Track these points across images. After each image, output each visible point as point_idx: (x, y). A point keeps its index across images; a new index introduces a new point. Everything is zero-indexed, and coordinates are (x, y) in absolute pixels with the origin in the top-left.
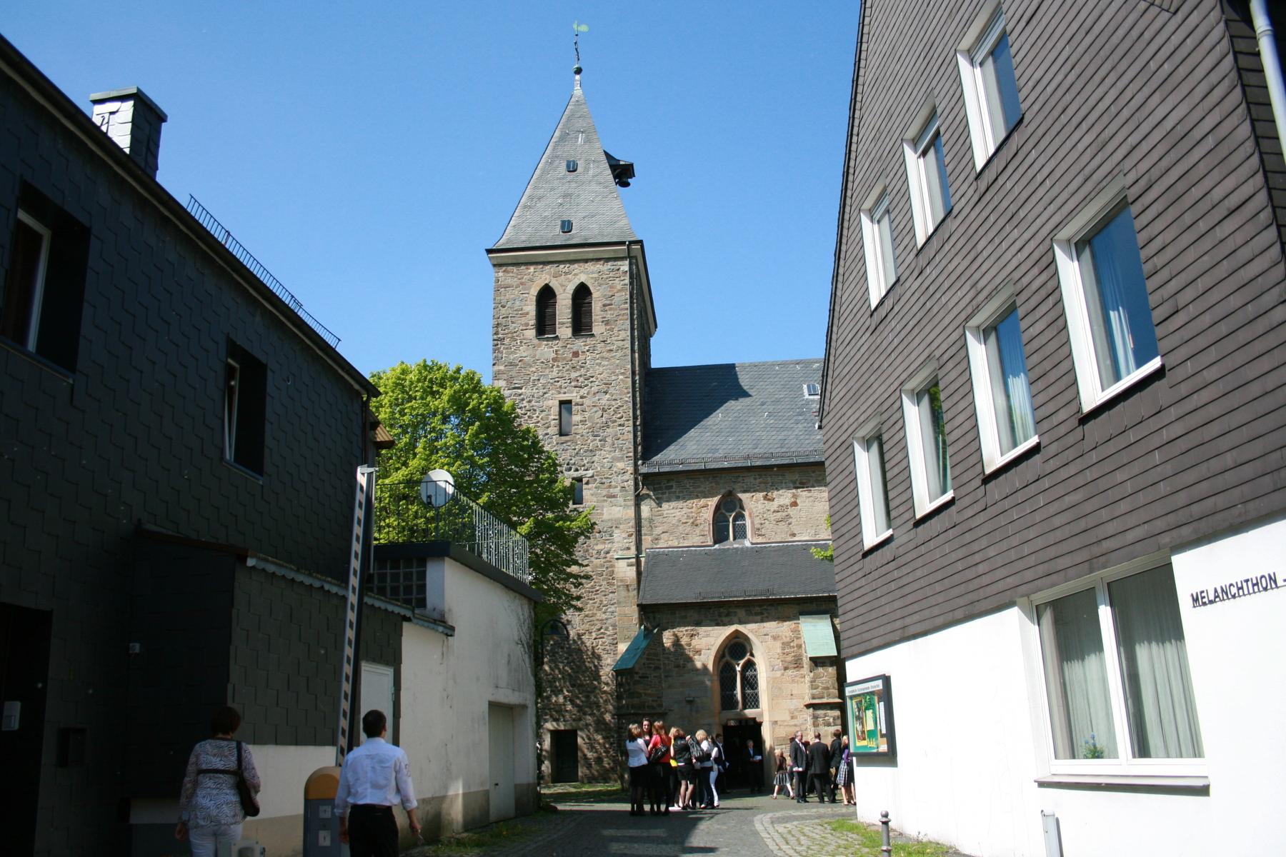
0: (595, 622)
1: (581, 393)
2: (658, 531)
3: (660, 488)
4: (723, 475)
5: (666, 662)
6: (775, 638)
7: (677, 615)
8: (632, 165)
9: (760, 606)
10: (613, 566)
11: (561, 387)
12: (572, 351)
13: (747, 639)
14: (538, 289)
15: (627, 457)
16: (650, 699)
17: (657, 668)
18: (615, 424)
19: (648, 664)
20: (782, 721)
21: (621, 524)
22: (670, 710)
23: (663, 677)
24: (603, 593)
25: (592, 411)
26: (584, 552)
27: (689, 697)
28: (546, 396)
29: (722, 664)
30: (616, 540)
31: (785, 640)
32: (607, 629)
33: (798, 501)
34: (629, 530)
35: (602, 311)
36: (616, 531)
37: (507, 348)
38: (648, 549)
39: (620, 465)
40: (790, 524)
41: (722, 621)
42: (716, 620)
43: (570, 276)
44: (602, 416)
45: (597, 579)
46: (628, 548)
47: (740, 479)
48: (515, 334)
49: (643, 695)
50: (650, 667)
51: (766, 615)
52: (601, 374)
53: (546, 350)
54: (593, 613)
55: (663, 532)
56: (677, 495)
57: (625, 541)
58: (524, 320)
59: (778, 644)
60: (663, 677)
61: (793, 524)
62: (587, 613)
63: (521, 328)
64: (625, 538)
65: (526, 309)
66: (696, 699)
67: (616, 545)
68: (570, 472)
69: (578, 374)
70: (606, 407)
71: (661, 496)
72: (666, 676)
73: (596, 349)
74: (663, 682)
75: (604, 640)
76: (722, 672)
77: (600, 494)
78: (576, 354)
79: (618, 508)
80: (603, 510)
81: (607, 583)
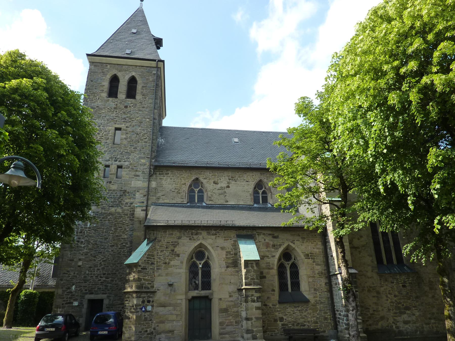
0: (121, 239)
1: (127, 125)
2: (159, 194)
3: (163, 174)
4: (194, 170)
5: (159, 260)
6: (223, 248)
7: (167, 233)
8: (162, 39)
11: (116, 121)
12: (124, 105)
13: (206, 248)
14: (111, 75)
16: (147, 282)
17: (152, 264)
18: (143, 141)
19: (147, 261)
21: (140, 190)
23: (156, 269)
24: (127, 225)
26: (119, 202)
27: (171, 282)
31: (228, 250)
32: (127, 244)
33: (230, 185)
36: (137, 193)
37: (91, 100)
39: (143, 161)
40: (225, 196)
42: (190, 237)
43: (127, 72)
45: (124, 217)
46: (143, 202)
50: (149, 263)
53: (112, 102)
56: (171, 177)
57: (141, 198)
58: (101, 89)
59: (224, 253)
60: (156, 269)
62: (117, 234)
63: (100, 92)
64: (141, 197)
65: (103, 83)
66: (174, 284)
68: (116, 162)
69: (126, 116)
70: (139, 133)
71: (162, 177)
72: (157, 269)
74: (155, 272)
75: (124, 249)
76: (190, 268)
77: (131, 174)
78: (126, 107)
79: (140, 182)
81: (130, 219)
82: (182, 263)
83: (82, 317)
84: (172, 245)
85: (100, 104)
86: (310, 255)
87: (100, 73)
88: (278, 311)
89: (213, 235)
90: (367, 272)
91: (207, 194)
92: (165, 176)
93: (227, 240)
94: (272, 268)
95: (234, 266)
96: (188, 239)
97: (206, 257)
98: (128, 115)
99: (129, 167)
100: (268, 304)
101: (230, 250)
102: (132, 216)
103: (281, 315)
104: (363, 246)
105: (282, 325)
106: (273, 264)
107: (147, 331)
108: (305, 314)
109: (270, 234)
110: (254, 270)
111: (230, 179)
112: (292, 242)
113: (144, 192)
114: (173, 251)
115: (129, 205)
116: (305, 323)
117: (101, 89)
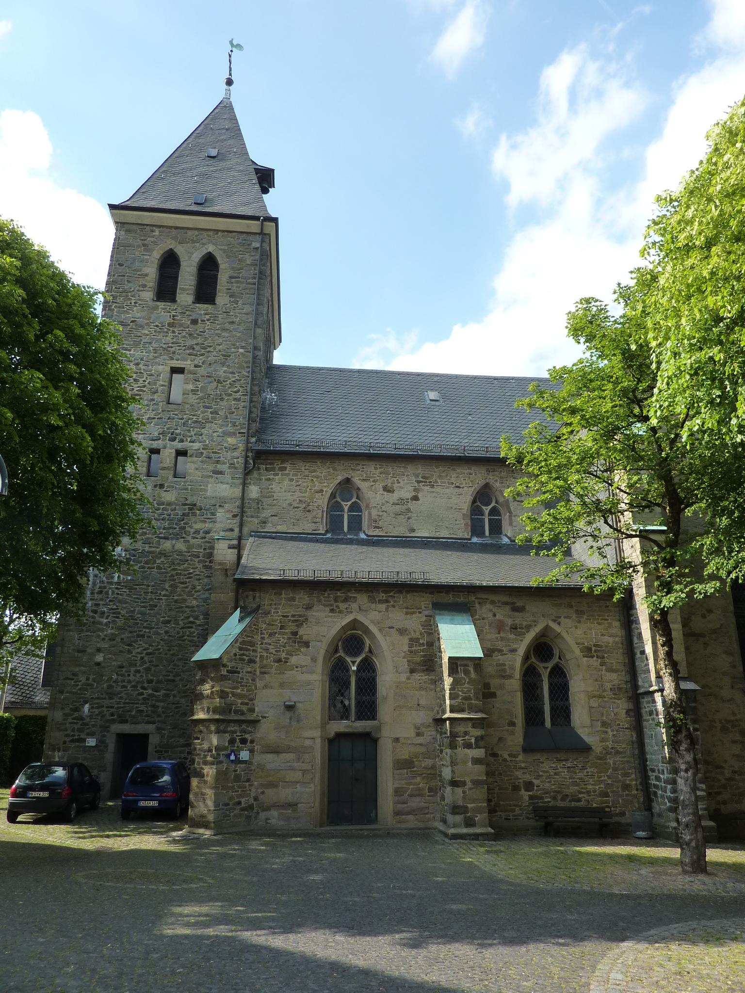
1: (196, 362)
2: (264, 514)
3: (273, 469)
6: (402, 632)
7: (283, 596)
8: (273, 170)
9: (385, 592)
10: (213, 548)
12: (191, 318)
15: (239, 433)
16: (240, 701)
17: (251, 661)
18: (231, 398)
19: (240, 655)
20: (405, 738)
22: (264, 717)
23: (258, 673)
25: (206, 381)
26: (180, 528)
28: (157, 360)
29: (526, 665)
30: (218, 520)
31: (414, 635)
32: (197, 618)
33: (419, 496)
34: (234, 510)
35: (228, 283)
36: (220, 510)
37: (119, 307)
38: (253, 532)
40: (409, 518)
41: (338, 607)
42: (332, 605)
44: (217, 388)
46: (232, 530)
47: (360, 467)
48: (130, 294)
49: (230, 695)
50: (244, 660)
51: (392, 603)
52: (219, 345)
53: (164, 312)
54: (182, 599)
55: (272, 516)
56: (291, 477)
58: (142, 281)
59: (405, 640)
60: (258, 673)
61: (413, 518)
62: (176, 598)
64: (228, 519)
66: (298, 705)
67: (218, 525)
68: (173, 443)
70: (222, 380)
73: (217, 319)
74: (257, 680)
76: (333, 671)
77: (206, 469)
80: (207, 486)
82: (314, 660)
83: (104, 771)
84: (293, 621)
85: (139, 315)
86: (593, 648)
87: (139, 246)
88: (521, 768)
89: (381, 602)
90: (721, 688)
91: (370, 514)
92: (277, 475)
93: (412, 613)
94: (510, 677)
95: (427, 670)
96: (328, 609)
97: (367, 649)
98: (200, 340)
99: (202, 453)
100: (500, 753)
101: (417, 635)
102: (208, 560)
103: (527, 777)
104: (713, 631)
105: (531, 797)
106: (512, 668)
107: (239, 803)
108: (580, 775)
109: (506, 603)
110: (470, 679)
111: (419, 482)
112: (554, 621)
113: (234, 507)
114: (295, 634)
115: (202, 535)
116: (581, 796)
117: (142, 281)
